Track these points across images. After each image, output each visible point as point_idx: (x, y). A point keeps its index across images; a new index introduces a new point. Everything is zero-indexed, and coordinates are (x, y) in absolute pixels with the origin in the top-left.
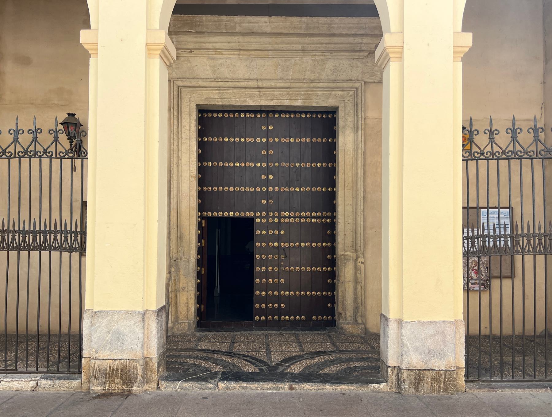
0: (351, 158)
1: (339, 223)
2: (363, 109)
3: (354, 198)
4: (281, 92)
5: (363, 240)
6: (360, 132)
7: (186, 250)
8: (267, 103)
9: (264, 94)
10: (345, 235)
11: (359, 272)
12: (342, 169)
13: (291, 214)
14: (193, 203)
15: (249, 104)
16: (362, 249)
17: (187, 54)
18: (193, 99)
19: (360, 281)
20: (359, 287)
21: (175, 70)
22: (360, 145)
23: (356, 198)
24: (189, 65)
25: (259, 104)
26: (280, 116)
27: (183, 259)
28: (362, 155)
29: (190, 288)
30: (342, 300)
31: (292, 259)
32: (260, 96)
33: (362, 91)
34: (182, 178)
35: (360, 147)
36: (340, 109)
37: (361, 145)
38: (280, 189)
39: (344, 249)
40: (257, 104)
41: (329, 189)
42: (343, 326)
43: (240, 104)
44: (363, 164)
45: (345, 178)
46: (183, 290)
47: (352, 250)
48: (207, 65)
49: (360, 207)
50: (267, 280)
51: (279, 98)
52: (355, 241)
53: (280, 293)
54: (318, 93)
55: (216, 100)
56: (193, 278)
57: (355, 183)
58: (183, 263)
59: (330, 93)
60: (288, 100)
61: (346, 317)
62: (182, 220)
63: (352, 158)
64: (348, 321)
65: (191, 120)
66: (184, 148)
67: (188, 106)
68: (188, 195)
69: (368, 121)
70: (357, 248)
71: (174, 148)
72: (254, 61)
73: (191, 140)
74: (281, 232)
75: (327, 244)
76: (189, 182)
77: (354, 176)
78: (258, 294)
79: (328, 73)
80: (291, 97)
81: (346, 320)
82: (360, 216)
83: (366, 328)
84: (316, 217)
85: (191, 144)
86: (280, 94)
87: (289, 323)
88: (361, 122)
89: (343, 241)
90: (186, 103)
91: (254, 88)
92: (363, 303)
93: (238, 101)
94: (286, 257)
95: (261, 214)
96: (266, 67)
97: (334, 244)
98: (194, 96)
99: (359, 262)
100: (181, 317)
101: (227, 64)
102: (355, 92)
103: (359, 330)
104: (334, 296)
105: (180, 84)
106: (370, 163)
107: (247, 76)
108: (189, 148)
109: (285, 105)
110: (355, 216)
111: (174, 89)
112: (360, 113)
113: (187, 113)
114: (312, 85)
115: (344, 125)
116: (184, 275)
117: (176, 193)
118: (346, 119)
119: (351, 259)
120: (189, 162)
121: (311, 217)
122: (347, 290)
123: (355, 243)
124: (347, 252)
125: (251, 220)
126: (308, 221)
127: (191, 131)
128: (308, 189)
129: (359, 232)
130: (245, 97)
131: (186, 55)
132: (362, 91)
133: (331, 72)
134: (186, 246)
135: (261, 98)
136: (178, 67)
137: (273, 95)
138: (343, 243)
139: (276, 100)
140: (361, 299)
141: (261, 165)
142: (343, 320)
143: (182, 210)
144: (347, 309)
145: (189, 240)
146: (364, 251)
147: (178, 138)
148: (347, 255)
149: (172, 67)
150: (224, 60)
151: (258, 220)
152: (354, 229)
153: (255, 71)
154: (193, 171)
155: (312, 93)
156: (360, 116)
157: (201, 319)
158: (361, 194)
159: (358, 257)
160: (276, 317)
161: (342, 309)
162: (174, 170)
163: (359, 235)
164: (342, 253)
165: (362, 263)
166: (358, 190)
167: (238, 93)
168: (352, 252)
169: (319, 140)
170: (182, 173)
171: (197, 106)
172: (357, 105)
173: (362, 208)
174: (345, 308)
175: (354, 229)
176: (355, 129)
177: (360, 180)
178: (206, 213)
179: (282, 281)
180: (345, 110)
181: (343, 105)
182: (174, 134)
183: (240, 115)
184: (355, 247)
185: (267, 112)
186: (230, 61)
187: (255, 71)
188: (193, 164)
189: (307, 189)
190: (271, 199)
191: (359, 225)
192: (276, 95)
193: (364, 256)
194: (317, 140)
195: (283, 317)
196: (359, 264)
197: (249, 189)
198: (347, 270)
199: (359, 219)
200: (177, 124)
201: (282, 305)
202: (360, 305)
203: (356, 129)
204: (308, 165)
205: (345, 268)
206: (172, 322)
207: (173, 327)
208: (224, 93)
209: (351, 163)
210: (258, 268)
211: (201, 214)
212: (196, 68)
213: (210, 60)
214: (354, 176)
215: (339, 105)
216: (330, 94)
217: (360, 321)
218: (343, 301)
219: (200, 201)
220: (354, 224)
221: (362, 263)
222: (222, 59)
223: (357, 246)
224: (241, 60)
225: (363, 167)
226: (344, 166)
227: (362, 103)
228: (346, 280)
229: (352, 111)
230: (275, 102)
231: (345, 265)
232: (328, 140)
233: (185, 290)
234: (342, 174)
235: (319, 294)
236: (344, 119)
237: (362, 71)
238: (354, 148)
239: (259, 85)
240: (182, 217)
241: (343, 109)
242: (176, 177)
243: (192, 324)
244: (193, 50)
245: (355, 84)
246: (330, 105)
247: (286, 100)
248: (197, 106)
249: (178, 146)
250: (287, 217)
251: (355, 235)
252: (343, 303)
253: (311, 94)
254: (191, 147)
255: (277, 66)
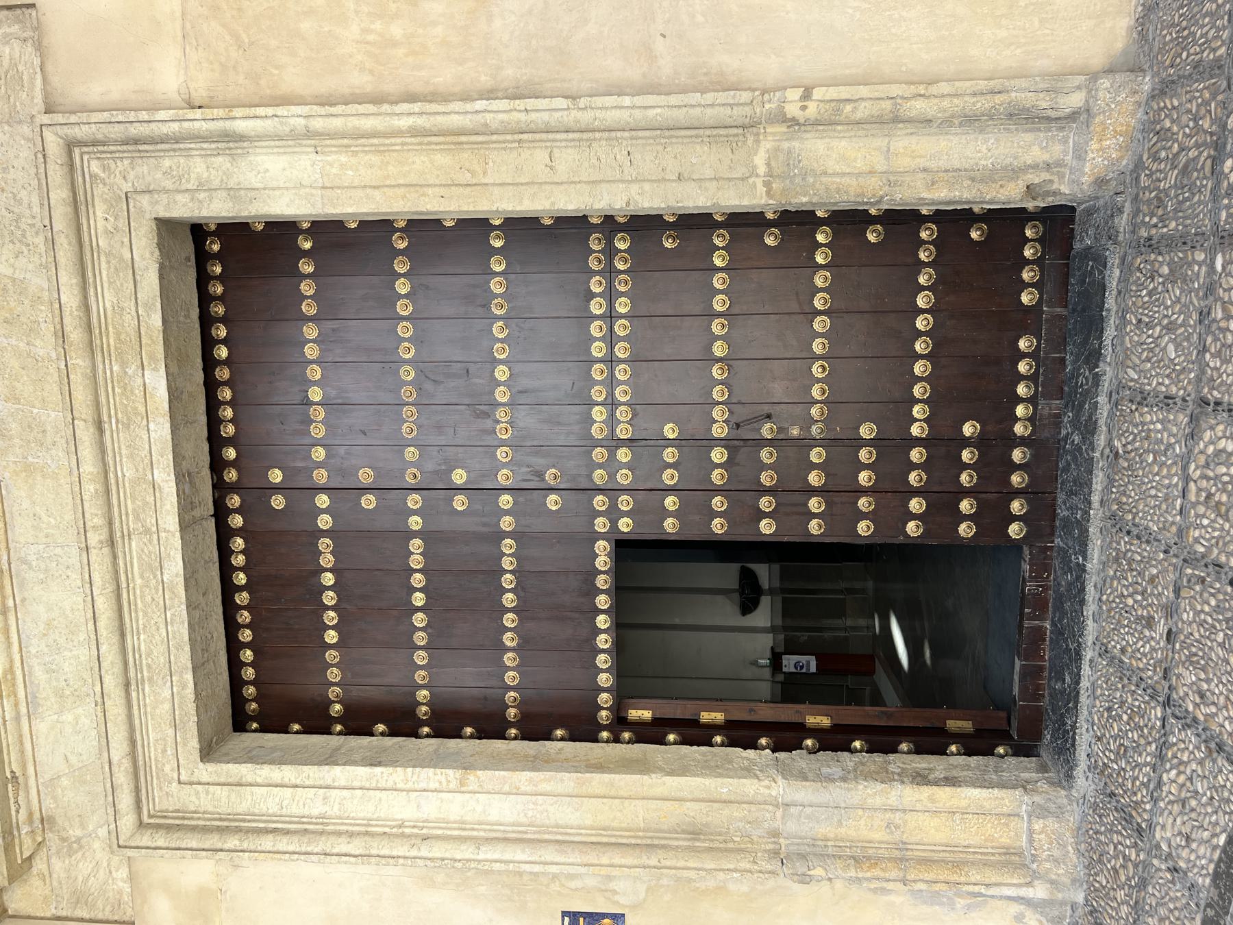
0: (354, 160)
1: (628, 203)
2: (144, 115)
3: (520, 141)
4: (124, 452)
5: (702, 93)
6: (241, 126)
7: (737, 812)
8: (168, 507)
9: (137, 518)
10: (680, 178)
11: (849, 108)
12: (404, 197)
13: (600, 399)
14: (562, 780)
15: (182, 573)
16: (745, 96)
17: (27, 792)
18: (183, 771)
19: (887, 105)
20: (918, 107)
21: (91, 828)
22: (292, 121)
23: (521, 134)
24: (65, 782)
25: (178, 535)
26: (231, 442)
27: (778, 824)
28: (333, 110)
29: (889, 802)
30: (967, 183)
31: (778, 390)
32: (147, 532)
33: (73, 119)
34: (468, 818)
35: (302, 121)
36: (163, 214)
37: (295, 118)
38: (503, 443)
39: (743, 179)
40: (177, 542)
41: (498, 244)
42: (1092, 179)
43: (184, 607)
44: (371, 108)
45: (437, 182)
46: (897, 827)
47: (745, 142)
48: (58, 721)
49: (557, 115)
50: (863, 491)
51: (147, 461)
52: (708, 132)
53: (917, 442)
54: (108, 305)
55: (179, 693)
56: (849, 790)
57: (454, 137)
58: (791, 827)
59: (103, 259)
60: (152, 426)
61: (1048, 166)
62: (624, 825)
63: (355, 153)
64: (1065, 152)
65: (259, 780)
66: (359, 807)
67: (207, 792)
68: (534, 798)
69: (200, 91)
70: (740, 122)
71: (357, 853)
72: (23, 555)
73: (329, 782)
74: (671, 437)
75: (719, 248)
76: (482, 797)
77: (429, 143)
78: (918, 527)
79: (31, 267)
80: (137, 414)
81: (1060, 164)
82: (598, 114)
83: (1110, 71)
84: (611, 295)
85: (343, 783)
86: (131, 457)
87: (1041, 401)
88: (199, 123)
89: (708, 184)
90: (199, 799)
91: (115, 557)
92: (996, 84)
93: (173, 615)
94: (769, 416)
95: (600, 514)
96: (38, 508)
97: (719, 218)
98: (172, 770)
99: (804, 108)
100: (1005, 840)
101: (46, 650)
102: (85, 149)
103: (1119, 103)
104: (941, 217)
105: (127, 822)
106: (371, 72)
107: (76, 579)
108: (359, 792)
109: (169, 437)
110: (597, 135)
111: (149, 844)
112: (165, 129)
113: (233, 796)
114: (75, 335)
115: (224, 194)
116: (840, 822)
117: (523, 851)
118: (200, 184)
119: (786, 145)
120: (408, 791)
121: (611, 316)
122: (923, 163)
123: (715, 132)
124: (755, 167)
125: (624, 548)
126: (625, 327)
127: (298, 782)
128: (498, 331)
129: (668, 113)
130: (157, 590)
131: (34, 792)
132: (73, 119)
133: (26, 252)
134: (726, 812)
135: (154, 529)
136: (77, 820)
137: (137, 481)
138: (715, 183)
139: (156, 472)
140: (974, 94)
141: (415, 513)
142: (1061, 176)
143: (588, 822)
144: (1008, 161)
145: (702, 800)
146: (754, 90)
147: (322, 833)
148: (768, 165)
149: (81, 838)
150: (34, 662)
151: (625, 525)
152: (654, 138)
153: (58, 551)
154: (444, 781)
155: (110, 329)
156: (175, 126)
157: (1002, 736)
158: (498, 112)
159: (781, 118)
160: (1017, 455)
161: (1012, 185)
162: (438, 855)
163: (680, 115)
164: (761, 190)
165: (807, 95)
166: (486, 125)
167: (145, 614)
168: (758, 141)
169: (307, 288)
170: (452, 818)
171: (208, 752)
172: (136, 141)
173: (561, 103)
174: (1004, 168)
175: (654, 138)
176: (231, 145)
177: (440, 119)
178: (604, 713)
179: (867, 431)
180: (167, 191)
181: (145, 201)
182: (309, 849)
183: (241, 589)
184: (735, 131)
185: (220, 488)
186: (34, 641)
187: (58, 551)
188: (415, 777)
189: (501, 336)
190: (540, 475)
191: (638, 114)
192: (137, 471)
193: (775, 90)
194: (308, 297)
195: (1019, 429)
196: (812, 109)
197: (509, 555)
198: (833, 166)
199: (612, 117)
200: (271, 836)
201: (968, 429)
202: (998, 99)
203: (232, 141)
204: (405, 330)
205: (825, 173)
206: (1029, 884)
207: (1052, 882)
208: (149, 666)
209: (375, 159)
210: (814, 527)
211: (605, 728)
212: (73, 759)
213: (40, 710)
214: (429, 143)
215: (148, 216)
216: (109, 255)
217: (1076, 100)
218: (973, 179)
219: (559, 733)
220: (632, 138)
221: (807, 95)
222: (31, 667)
223: (730, 122)
224: (23, 600)
225: (386, 107)
226: (390, 192)
227: (120, 118)
228: (881, 165)
229: (167, 163)
230: (164, 476)
231: (814, 173)
232: (306, 254)
233: (898, 821)
234: (424, 195)
235: (929, 280)
236: (202, 196)
237: (8, 123)
238: (312, 149)
239: (101, 542)
240: (615, 824)
241: (164, 198)
242: (463, 847)
243: (1037, 799)
244: (9, 775)
245: (49, 152)
246: (152, 254)
247: (153, 435)
248: (208, 752)
249: (351, 835)
250: (612, 415)
251: (683, 133)
252: (982, 181)
253: (118, 334)
254: (356, 784)
255: (29, 470)
